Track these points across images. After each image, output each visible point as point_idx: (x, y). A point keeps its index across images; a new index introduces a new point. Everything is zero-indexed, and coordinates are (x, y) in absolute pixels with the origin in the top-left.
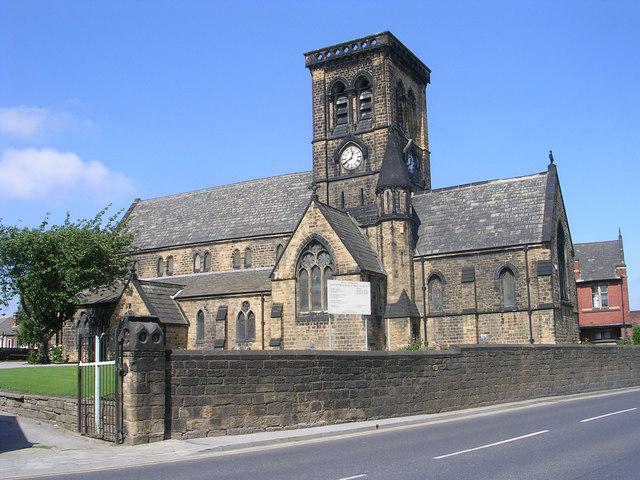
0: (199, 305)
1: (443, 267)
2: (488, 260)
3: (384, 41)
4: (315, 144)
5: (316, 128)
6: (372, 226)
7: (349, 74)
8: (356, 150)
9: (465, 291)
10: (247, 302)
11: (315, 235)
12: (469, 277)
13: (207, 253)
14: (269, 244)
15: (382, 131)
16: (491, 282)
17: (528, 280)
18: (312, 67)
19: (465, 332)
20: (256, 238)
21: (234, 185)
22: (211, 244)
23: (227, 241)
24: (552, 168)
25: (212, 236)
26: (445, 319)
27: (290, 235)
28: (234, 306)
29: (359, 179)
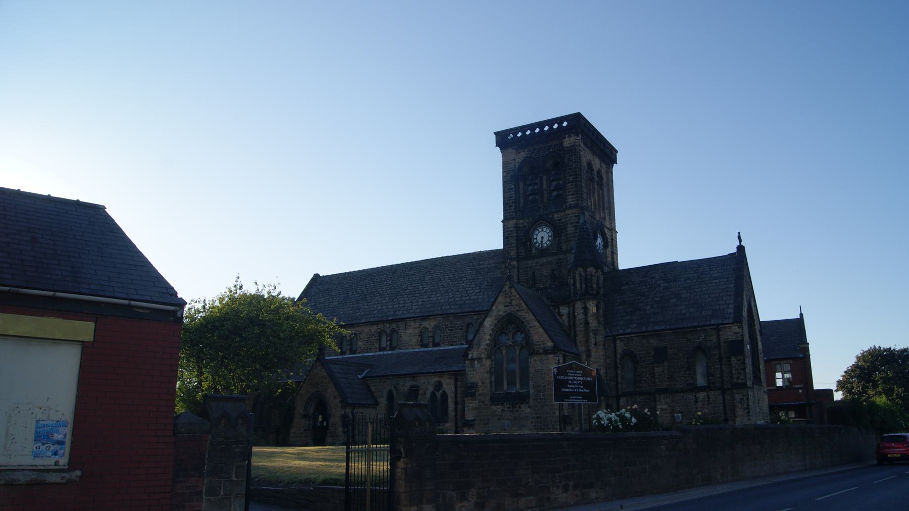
13: (393, 331)
15: (574, 211)
23: (415, 319)
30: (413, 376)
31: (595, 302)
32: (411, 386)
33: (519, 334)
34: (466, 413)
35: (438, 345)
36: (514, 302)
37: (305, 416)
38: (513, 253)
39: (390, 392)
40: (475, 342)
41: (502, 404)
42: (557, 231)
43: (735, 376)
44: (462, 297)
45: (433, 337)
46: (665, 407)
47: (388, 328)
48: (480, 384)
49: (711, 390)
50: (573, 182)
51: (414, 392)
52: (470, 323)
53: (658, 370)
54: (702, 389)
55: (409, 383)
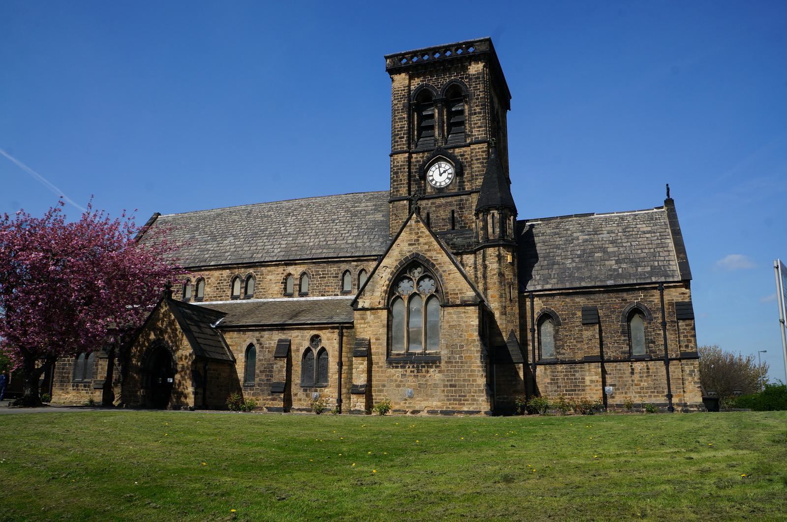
0: (250, 338)
1: (557, 305)
2: (614, 299)
3: (484, 48)
4: (395, 156)
6: (467, 253)
7: (439, 83)
8: (445, 166)
9: (587, 334)
10: (317, 336)
12: (591, 318)
14: (333, 269)
15: (480, 146)
16: (617, 326)
17: (664, 324)
18: (393, 71)
19: (588, 383)
21: (280, 202)
22: (257, 266)
23: (278, 264)
24: (669, 202)
25: (258, 257)
26: (560, 368)
27: (380, 258)
28: (300, 340)
29: (449, 199)
32: (280, 341)
34: (354, 375)
35: (306, 295)
36: (421, 240)
39: (251, 346)
43: (683, 344)
44: (336, 240)
45: (300, 285)
46: (595, 378)
47: (243, 272)
49: (652, 360)
50: (480, 113)
51: (284, 351)
52: (347, 271)
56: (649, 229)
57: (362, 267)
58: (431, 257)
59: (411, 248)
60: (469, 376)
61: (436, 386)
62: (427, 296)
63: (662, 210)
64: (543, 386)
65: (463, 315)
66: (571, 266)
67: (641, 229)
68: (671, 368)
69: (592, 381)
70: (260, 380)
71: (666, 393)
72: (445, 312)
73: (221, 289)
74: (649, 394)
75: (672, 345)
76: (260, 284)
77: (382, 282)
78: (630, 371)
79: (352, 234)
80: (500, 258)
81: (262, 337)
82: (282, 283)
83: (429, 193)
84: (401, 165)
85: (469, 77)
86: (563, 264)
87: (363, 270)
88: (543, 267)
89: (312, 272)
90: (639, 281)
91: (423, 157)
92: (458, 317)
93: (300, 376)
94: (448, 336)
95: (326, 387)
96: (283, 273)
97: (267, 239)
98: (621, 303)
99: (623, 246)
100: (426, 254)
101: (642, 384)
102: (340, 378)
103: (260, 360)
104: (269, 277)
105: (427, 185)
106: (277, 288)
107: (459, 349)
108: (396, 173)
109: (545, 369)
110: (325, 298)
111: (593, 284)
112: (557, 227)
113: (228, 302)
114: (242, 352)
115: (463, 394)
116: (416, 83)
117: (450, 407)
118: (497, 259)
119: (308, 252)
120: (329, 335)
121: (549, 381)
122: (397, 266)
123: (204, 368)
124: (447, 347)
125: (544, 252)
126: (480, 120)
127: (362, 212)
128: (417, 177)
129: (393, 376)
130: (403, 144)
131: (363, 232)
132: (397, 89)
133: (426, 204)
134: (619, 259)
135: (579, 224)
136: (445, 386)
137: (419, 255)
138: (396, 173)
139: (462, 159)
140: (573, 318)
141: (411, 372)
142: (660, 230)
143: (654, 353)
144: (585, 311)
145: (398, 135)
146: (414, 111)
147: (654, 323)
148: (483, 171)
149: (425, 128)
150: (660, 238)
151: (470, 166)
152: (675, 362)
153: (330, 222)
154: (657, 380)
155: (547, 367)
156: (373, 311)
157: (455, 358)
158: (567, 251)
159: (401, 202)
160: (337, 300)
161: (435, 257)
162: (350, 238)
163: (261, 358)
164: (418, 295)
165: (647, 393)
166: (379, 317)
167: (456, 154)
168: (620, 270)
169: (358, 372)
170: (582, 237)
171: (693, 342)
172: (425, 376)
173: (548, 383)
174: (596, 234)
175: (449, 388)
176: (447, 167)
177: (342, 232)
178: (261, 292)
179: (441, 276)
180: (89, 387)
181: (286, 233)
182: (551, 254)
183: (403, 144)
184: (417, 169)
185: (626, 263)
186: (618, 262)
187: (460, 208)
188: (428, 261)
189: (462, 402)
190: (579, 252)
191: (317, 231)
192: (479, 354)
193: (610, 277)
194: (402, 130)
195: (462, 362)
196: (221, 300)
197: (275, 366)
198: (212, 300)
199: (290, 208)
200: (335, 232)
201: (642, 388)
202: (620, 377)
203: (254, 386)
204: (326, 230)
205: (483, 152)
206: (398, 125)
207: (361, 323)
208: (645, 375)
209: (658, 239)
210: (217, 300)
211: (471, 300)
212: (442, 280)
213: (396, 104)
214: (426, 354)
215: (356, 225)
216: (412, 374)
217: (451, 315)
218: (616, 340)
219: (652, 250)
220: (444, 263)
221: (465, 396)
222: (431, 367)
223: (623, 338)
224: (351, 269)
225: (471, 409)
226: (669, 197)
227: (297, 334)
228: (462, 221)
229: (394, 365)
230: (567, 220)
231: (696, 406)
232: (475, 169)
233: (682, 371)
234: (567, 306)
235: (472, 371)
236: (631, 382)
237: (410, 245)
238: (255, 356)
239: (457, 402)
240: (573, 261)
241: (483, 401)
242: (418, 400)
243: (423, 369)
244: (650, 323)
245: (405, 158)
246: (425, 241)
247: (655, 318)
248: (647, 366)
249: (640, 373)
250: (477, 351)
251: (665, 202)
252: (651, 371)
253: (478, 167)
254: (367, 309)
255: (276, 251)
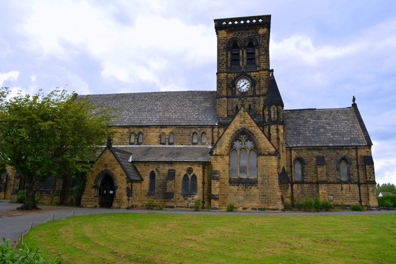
0: (151, 168)
1: (304, 154)
2: (333, 153)
4: (220, 74)
5: (221, 65)
7: (243, 36)
11: (244, 129)
13: (140, 133)
14: (188, 131)
15: (265, 72)
16: (334, 166)
17: (357, 166)
20: (179, 127)
23: (156, 126)
25: (144, 123)
26: (305, 185)
30: (171, 163)
31: (282, 126)
33: (249, 141)
35: (172, 144)
36: (247, 121)
37: (95, 187)
38: (224, 93)
40: (218, 144)
41: (238, 185)
42: (253, 83)
43: (368, 177)
45: (169, 139)
46: (324, 191)
47: (136, 131)
48: (222, 171)
49: (352, 183)
50: (264, 55)
53: (320, 169)
54: (345, 183)
55: (167, 168)
56: (346, 118)
57: (203, 131)
58: (252, 130)
59: (241, 125)
60: (272, 191)
61: (255, 195)
62: (249, 150)
63: (351, 109)
64: (297, 194)
65: (269, 160)
66: (309, 135)
67: (342, 118)
68: (362, 188)
69: (322, 193)
70: (158, 191)
71: (359, 200)
72: (260, 158)
73: (123, 139)
74: (351, 200)
75: (362, 176)
76: (146, 137)
77: (226, 142)
78: (341, 188)
79: (195, 113)
80: (278, 130)
81: (159, 168)
82: (159, 137)
83: (237, 94)
84: (223, 79)
85: (258, 35)
86: (305, 134)
87: (204, 132)
88: (295, 135)
89: (176, 132)
90: (345, 145)
91: (234, 76)
92: (266, 161)
93: (181, 189)
94: (261, 171)
95: (196, 195)
96: (159, 132)
97: (147, 113)
98: (336, 155)
99: (334, 126)
100: (249, 128)
101: (347, 195)
102: (203, 190)
103: (158, 180)
104: (151, 134)
105: (236, 90)
106: (156, 140)
107: (267, 177)
108: (220, 83)
109: (298, 186)
110: (184, 146)
111: (322, 145)
112: (298, 115)
113: (128, 146)
114: (147, 175)
115: (269, 200)
116: (231, 35)
117: (263, 206)
118: (276, 131)
119: (173, 122)
120: (197, 168)
121: (300, 192)
122: (234, 133)
123: (131, 185)
124: (261, 176)
125: (294, 127)
126: (264, 59)
127: (198, 102)
128: (231, 86)
129: (233, 190)
130: (224, 68)
131: (201, 112)
132: (220, 38)
133: (236, 100)
134: (333, 133)
135: (309, 114)
136: (260, 196)
137: (245, 128)
138: (220, 83)
139: (255, 78)
140: (312, 161)
141: (242, 188)
142: (352, 119)
143: (353, 180)
144: (318, 158)
145: (221, 63)
146: (229, 50)
147: (353, 165)
148: (266, 85)
149: (235, 60)
150: (352, 123)
151: (259, 82)
152: (363, 185)
153: (181, 106)
154: (354, 193)
155: (299, 185)
156: (221, 156)
157: (265, 182)
158: (306, 127)
159: (223, 99)
160: (191, 147)
161: (254, 130)
162: (195, 115)
163: (159, 179)
164: (245, 149)
165: (349, 200)
166: (224, 160)
167: (252, 75)
168: (335, 139)
169: (214, 188)
170: (312, 121)
171: (373, 175)
172: (249, 191)
173: (299, 193)
174: (319, 119)
175: (262, 197)
176: (247, 82)
177: (190, 112)
178: (147, 141)
179: (257, 140)
180: (49, 193)
181: (158, 110)
182: (298, 129)
183: (224, 68)
184: (231, 81)
185: (337, 135)
186: (333, 134)
187: (254, 103)
188: (250, 132)
189: (269, 204)
190: (312, 128)
191: (175, 110)
192: (277, 180)
193: (330, 142)
194: (223, 61)
195: (269, 184)
196: (123, 145)
197: (167, 184)
198: (118, 145)
199: (157, 97)
200: (186, 112)
201: (347, 197)
202: (336, 191)
203: (154, 194)
204: (180, 110)
205: (266, 75)
206: (221, 58)
207: (214, 163)
208: (348, 191)
209: (351, 124)
210: (121, 145)
211: (273, 153)
212: (258, 142)
213: (220, 47)
214: (249, 179)
215: (197, 108)
216: (243, 189)
217: (263, 160)
218: (333, 173)
219: (349, 129)
220: (259, 133)
221: (271, 201)
222: (253, 186)
223: (337, 172)
224: (197, 132)
225: (274, 208)
226: (354, 102)
227: (179, 167)
228: (254, 110)
229: (233, 184)
230: (302, 111)
231: (375, 207)
232: (262, 84)
233: (368, 190)
234: (309, 155)
235: (274, 188)
236: (341, 194)
237: (240, 123)
238: (155, 178)
239: (267, 204)
240: (310, 133)
241: (280, 204)
242: (246, 203)
243: (249, 187)
244: (351, 165)
245: (225, 76)
246: (248, 122)
247: (353, 163)
248: (349, 186)
249: (346, 189)
250: (277, 179)
251: (352, 105)
252: (351, 189)
253: (264, 83)
254: (218, 155)
255: (154, 120)
